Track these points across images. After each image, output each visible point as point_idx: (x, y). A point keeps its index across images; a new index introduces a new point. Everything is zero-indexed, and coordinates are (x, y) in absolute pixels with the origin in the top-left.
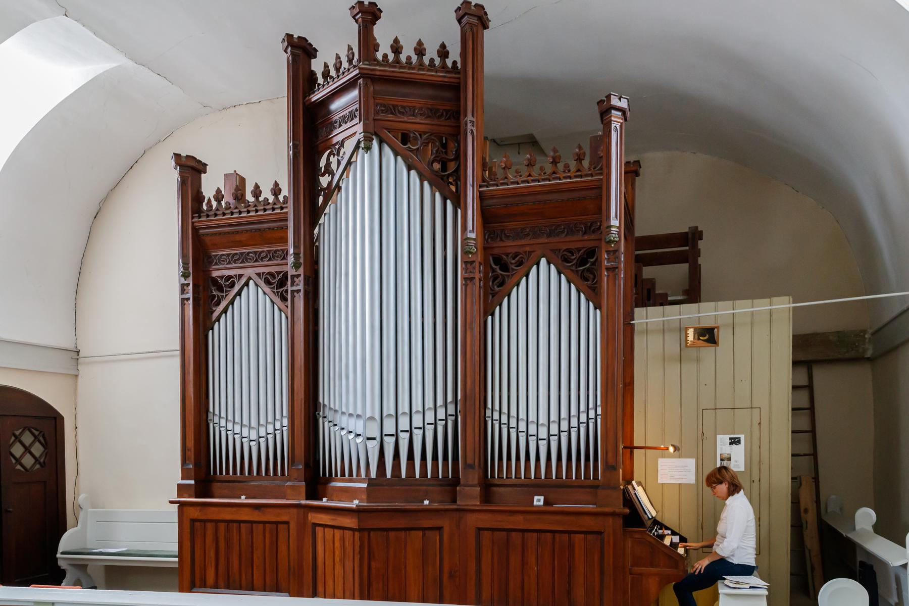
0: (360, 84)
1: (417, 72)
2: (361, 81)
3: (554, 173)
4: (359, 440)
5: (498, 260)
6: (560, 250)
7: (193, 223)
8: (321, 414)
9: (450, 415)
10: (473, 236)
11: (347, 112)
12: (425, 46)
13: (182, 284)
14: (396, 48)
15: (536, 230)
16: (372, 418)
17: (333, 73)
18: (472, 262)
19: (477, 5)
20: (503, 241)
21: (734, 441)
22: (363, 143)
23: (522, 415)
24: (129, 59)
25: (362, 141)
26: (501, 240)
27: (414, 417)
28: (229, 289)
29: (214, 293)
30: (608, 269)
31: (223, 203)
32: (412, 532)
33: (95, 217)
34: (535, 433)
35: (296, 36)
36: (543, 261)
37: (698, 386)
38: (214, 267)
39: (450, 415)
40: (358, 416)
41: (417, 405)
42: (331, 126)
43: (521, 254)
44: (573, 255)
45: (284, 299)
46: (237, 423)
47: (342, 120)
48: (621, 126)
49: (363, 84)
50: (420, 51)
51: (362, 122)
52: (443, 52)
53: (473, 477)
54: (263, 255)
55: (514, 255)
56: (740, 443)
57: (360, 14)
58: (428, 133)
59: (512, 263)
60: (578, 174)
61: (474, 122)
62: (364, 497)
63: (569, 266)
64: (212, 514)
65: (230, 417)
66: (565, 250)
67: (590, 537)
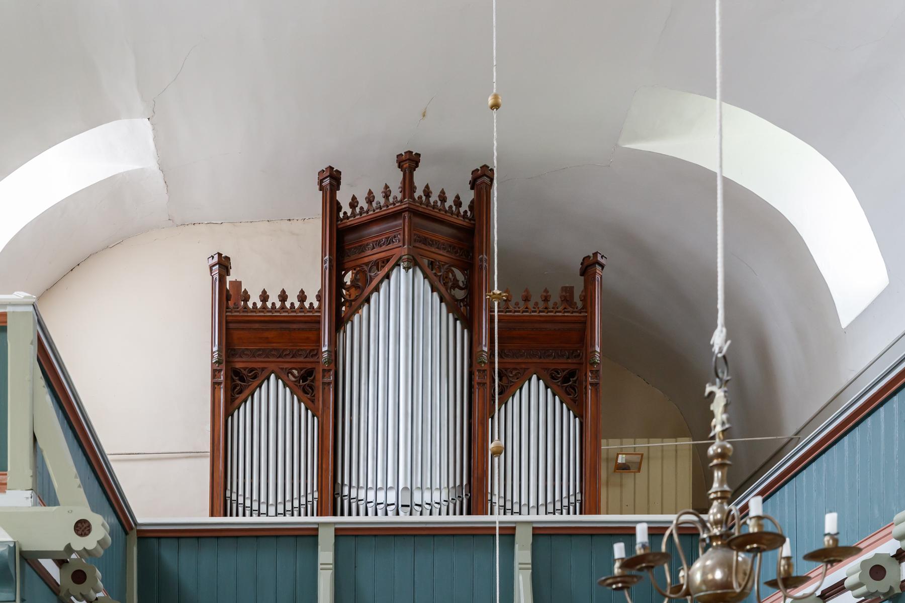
2: (406, 214)
6: (549, 369)
12: (446, 195)
13: (214, 370)
14: (427, 192)
15: (304, 352)
18: (484, 371)
23: (516, 499)
30: (591, 384)
34: (257, 509)
36: (534, 377)
41: (436, 484)
43: (256, 370)
44: (559, 374)
50: (443, 198)
51: (406, 246)
59: (510, 376)
66: (553, 370)
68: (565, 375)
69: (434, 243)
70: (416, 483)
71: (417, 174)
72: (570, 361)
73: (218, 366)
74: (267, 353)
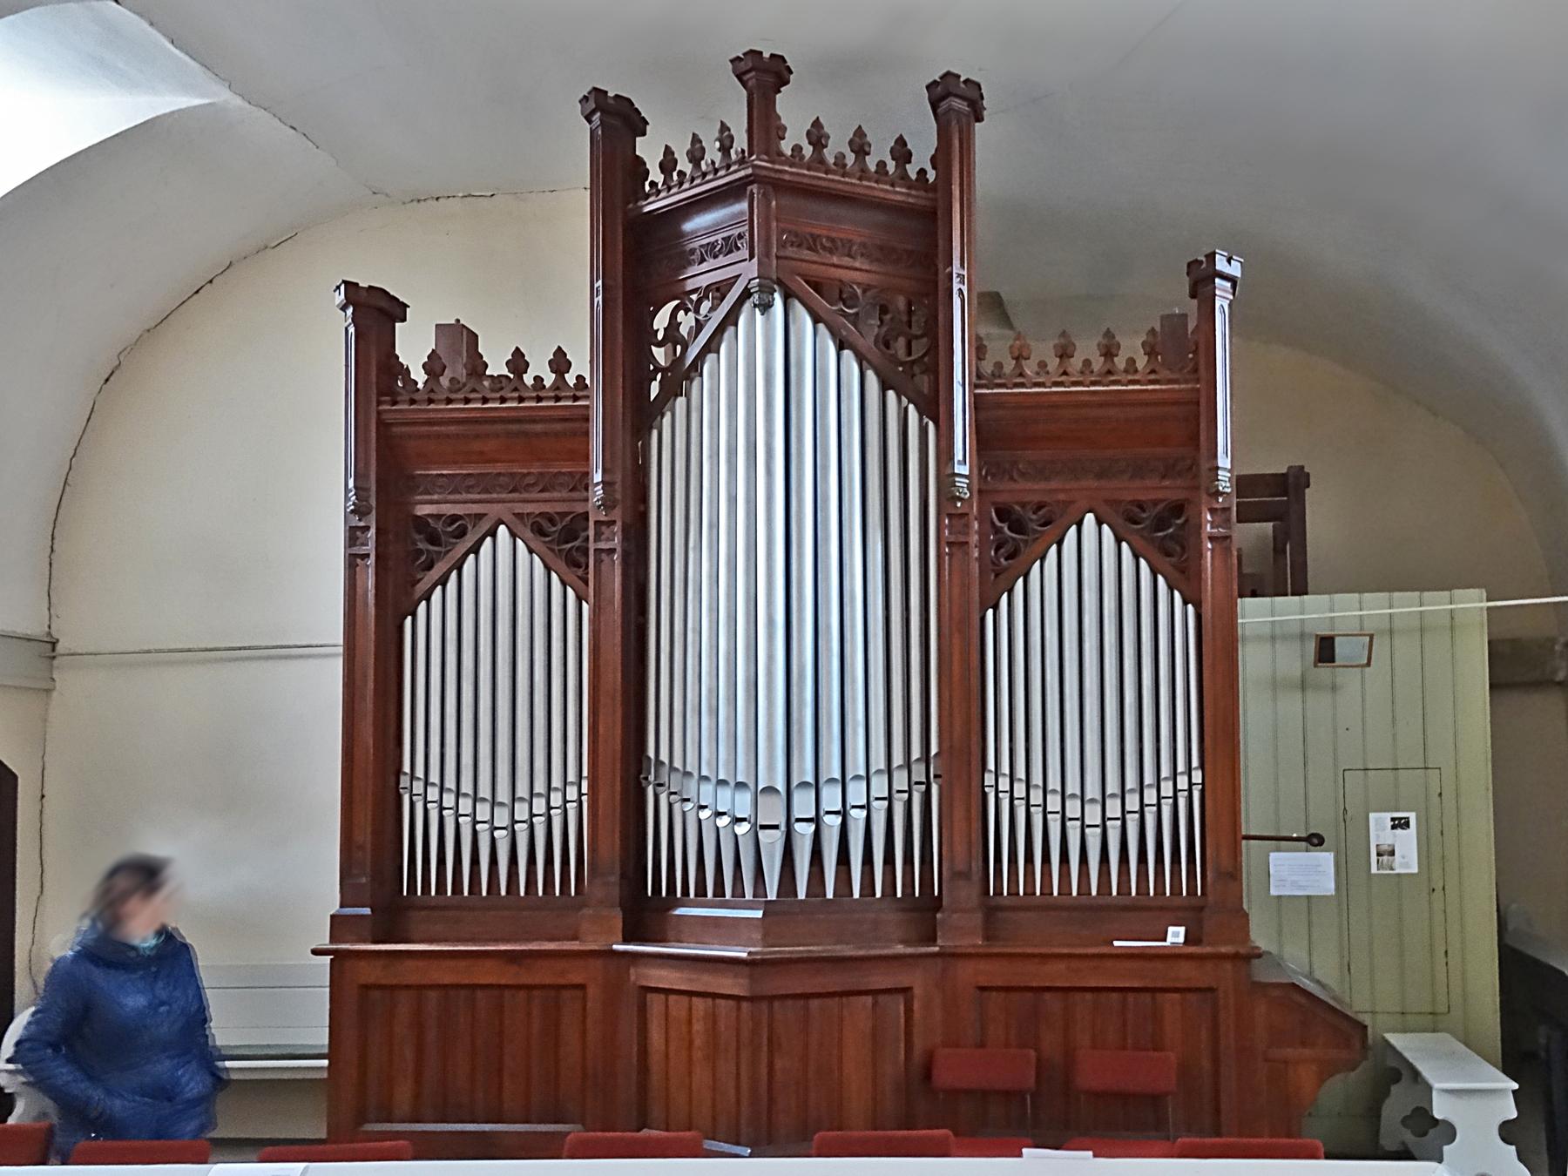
0: (752, 194)
1: (824, 176)
3: (1109, 372)
4: (742, 829)
5: (1003, 513)
6: (1121, 502)
7: (379, 413)
8: (652, 778)
9: (917, 783)
10: (965, 470)
11: (719, 237)
12: (869, 139)
14: (817, 136)
16: (770, 790)
17: (684, 165)
19: (967, 81)
20: (1015, 481)
21: (1400, 822)
22: (756, 296)
24: (235, 93)
25: (756, 292)
26: (1012, 478)
27: (851, 787)
28: (454, 540)
29: (421, 546)
30: (1212, 538)
31: (444, 381)
32: (852, 999)
33: (107, 380)
35: (611, 94)
36: (1090, 518)
37: (1335, 731)
38: (419, 497)
39: (917, 783)
40: (740, 785)
41: (857, 765)
42: (685, 260)
45: (573, 562)
46: (466, 795)
47: (706, 252)
48: (1230, 305)
49: (758, 193)
50: (860, 146)
52: (902, 153)
53: (968, 893)
54: (530, 480)
55: (1035, 507)
56: (1409, 827)
57: (753, 73)
58: (875, 287)
59: (1031, 520)
60: (1152, 377)
61: (964, 276)
62: (757, 936)
63: (1138, 530)
64: (411, 974)
65: (450, 783)
66: (1132, 502)
67: (1190, 996)
68: (1159, 513)
69: (839, 244)
70: (802, 771)
71: (785, 104)
72: (1167, 483)
73: (360, 520)
74: (484, 484)
